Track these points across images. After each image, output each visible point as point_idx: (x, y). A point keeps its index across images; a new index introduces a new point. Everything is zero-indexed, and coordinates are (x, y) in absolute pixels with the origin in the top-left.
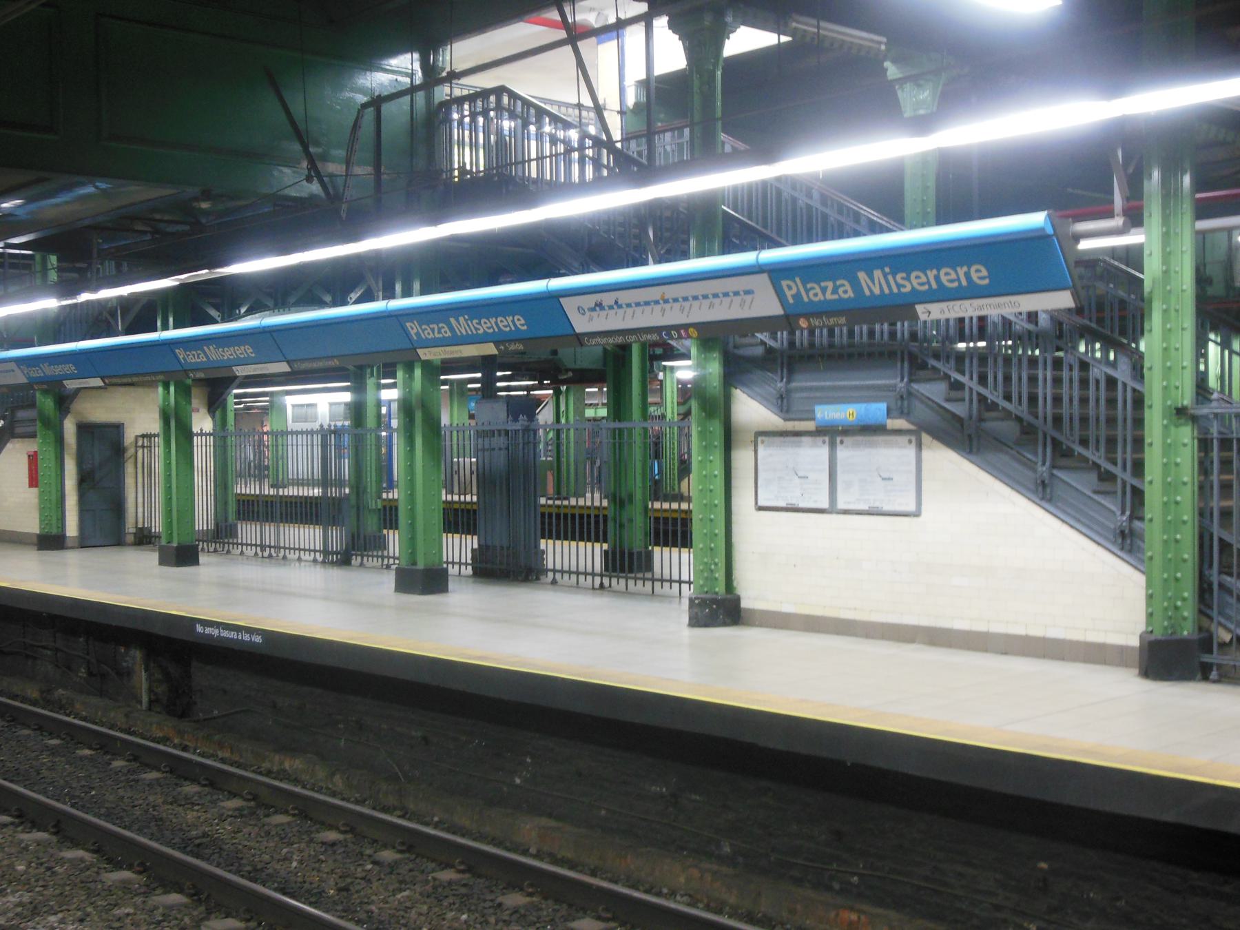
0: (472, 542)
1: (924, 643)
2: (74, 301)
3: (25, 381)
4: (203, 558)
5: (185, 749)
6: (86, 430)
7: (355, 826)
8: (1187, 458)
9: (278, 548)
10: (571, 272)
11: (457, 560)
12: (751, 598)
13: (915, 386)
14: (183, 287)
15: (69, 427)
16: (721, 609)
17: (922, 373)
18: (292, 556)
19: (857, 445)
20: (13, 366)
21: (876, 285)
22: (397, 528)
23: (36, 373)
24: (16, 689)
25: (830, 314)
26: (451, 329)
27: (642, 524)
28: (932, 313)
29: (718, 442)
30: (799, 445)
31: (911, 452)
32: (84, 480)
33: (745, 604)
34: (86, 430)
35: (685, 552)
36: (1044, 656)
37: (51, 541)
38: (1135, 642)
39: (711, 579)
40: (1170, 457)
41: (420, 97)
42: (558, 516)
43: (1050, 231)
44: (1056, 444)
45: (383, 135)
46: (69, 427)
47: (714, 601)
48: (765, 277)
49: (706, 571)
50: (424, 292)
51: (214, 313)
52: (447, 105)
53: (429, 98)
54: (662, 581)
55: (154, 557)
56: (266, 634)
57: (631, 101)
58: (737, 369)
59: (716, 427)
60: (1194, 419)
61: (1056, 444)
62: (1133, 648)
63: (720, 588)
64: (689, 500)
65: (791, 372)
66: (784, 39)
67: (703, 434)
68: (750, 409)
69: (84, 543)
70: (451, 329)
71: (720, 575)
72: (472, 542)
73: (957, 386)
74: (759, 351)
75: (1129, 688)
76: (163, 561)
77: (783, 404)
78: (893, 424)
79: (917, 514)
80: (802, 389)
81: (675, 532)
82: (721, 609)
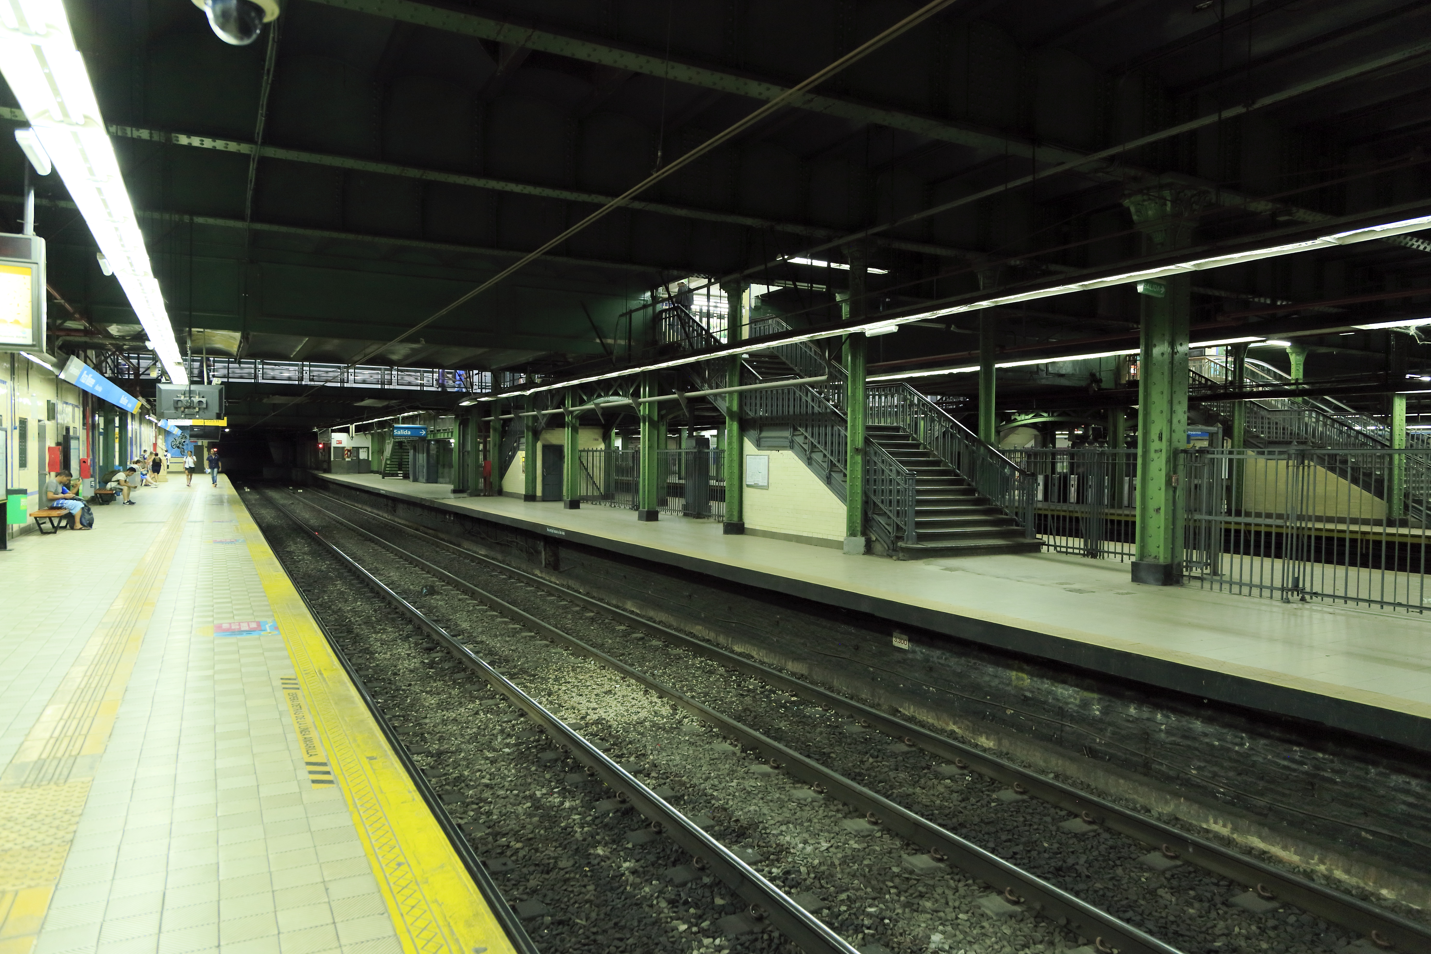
1: (355, 473)
4: (581, 505)
11: (1256, 580)
12: (748, 524)
17: (797, 433)
24: (475, 549)
33: (746, 526)
34: (545, 447)
37: (530, 497)
39: (732, 515)
42: (1071, 518)
45: (633, 324)
49: (730, 511)
53: (654, 310)
56: (566, 531)
57: (753, 305)
63: (735, 519)
65: (761, 431)
66: (773, 289)
69: (545, 499)
71: (736, 513)
72: (683, 501)
76: (640, 518)
79: (766, 488)
81: (719, 495)
82: (736, 527)
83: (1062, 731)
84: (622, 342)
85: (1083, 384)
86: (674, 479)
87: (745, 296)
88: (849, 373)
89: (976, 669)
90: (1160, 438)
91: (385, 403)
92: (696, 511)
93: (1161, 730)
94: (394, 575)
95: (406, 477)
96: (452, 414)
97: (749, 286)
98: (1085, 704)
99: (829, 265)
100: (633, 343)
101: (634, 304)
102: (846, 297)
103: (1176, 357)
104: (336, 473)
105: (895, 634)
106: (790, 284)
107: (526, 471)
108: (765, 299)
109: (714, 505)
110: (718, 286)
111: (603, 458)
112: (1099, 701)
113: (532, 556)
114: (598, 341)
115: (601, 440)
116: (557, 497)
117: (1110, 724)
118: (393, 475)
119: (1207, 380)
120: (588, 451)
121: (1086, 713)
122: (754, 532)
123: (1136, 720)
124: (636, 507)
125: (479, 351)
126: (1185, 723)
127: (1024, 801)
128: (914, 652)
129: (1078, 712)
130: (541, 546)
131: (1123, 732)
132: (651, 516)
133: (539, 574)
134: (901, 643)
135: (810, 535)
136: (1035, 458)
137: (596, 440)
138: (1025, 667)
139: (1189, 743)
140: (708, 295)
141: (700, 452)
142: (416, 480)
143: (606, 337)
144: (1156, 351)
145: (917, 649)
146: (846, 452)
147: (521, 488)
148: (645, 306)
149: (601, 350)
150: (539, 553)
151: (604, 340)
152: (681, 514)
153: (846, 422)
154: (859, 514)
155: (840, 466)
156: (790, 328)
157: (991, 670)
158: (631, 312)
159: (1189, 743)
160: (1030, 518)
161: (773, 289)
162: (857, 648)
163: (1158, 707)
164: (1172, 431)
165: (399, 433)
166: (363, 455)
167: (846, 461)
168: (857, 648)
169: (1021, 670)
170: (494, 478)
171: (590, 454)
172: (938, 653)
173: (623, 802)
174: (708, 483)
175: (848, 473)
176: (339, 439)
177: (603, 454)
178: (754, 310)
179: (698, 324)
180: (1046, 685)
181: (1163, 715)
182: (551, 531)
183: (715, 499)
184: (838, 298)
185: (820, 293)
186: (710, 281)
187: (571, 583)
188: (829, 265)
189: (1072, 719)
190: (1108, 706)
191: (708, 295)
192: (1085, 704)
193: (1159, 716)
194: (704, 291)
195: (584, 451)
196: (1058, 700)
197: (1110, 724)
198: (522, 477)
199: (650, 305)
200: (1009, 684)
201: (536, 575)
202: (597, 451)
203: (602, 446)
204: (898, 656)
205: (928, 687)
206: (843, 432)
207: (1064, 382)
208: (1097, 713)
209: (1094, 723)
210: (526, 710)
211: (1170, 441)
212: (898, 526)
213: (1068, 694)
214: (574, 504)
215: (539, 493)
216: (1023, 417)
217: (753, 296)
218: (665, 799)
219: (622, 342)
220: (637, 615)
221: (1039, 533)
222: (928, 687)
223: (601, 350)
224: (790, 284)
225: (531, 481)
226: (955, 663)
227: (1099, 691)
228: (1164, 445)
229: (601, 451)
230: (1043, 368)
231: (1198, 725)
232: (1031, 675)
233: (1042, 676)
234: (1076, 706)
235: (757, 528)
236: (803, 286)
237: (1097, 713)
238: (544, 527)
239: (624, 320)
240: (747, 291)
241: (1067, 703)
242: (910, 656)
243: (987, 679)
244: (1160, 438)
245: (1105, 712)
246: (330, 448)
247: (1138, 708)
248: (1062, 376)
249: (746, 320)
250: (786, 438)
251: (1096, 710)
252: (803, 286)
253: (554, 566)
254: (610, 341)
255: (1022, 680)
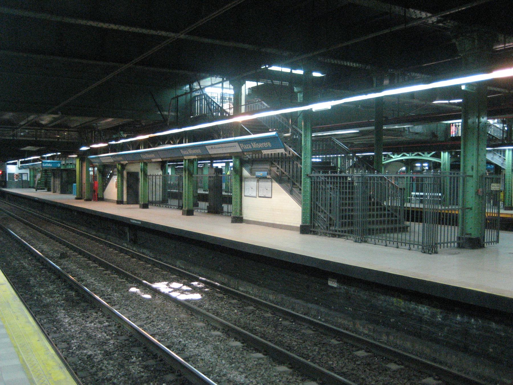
0: (207, 204)
2: (117, 143)
3: (240, 150)
4: (149, 207)
5: (160, 260)
6: (129, 173)
7: (155, 264)
8: (308, 185)
9: (228, 212)
10: (209, 140)
11: (449, 240)
12: (245, 217)
13: (272, 168)
14: (150, 138)
15: (125, 173)
16: (238, 219)
17: (273, 166)
18: (173, 207)
19: (263, 181)
20: (236, 144)
21: (255, 146)
22: (231, 204)
23: (248, 147)
25: (249, 152)
26: (252, 146)
27: (219, 200)
28: (265, 152)
29: (238, 180)
30: (267, 182)
31: (270, 183)
32: (128, 187)
33: (244, 218)
34: (129, 173)
35: (456, 227)
36: (281, 228)
37: (120, 202)
38: (299, 226)
40: (306, 184)
41: (189, 95)
43: (277, 136)
44: (293, 182)
46: (125, 173)
47: (237, 217)
48: (237, 143)
50: (144, 148)
51: (152, 146)
52: (195, 97)
54: (489, 242)
55: (229, 219)
56: (141, 221)
57: (247, 93)
58: (243, 163)
59: (238, 177)
60: (310, 177)
61: (293, 182)
62: (298, 227)
64: (231, 192)
65: (252, 164)
66: (259, 84)
67: (235, 178)
68: (246, 173)
69: (128, 203)
70: (252, 146)
72: (207, 204)
73: (278, 168)
74: (247, 159)
75: (297, 236)
76: (183, 214)
77: (251, 172)
78: (269, 177)
80: (254, 168)
81: (229, 200)
82: (238, 219)
83: (421, 330)
84: (173, 114)
85: (428, 138)
86: (200, 191)
87: (243, 87)
88: (303, 133)
89: (375, 297)
90: (472, 169)
91: (38, 148)
92: (215, 210)
93: (473, 328)
94: (45, 247)
95: (49, 190)
96: (76, 154)
97: (245, 83)
98: (434, 315)
99: (291, 71)
100: (179, 114)
101: (179, 92)
102: (300, 89)
103: (481, 124)
104: (9, 188)
105: (329, 279)
106: (269, 82)
107: (117, 186)
108: (253, 89)
109: (225, 207)
110: (228, 82)
111: (161, 180)
112: (441, 313)
113: (121, 236)
114: (159, 113)
115: (160, 169)
116: (136, 202)
117: (446, 325)
118: (41, 189)
119: (493, 136)
120: (153, 176)
121: (434, 320)
122: (249, 222)
123: (460, 323)
124: (180, 207)
125: (88, 119)
126: (486, 324)
127: (402, 369)
128: (340, 288)
129: (429, 319)
130: (127, 230)
131: (454, 330)
132: (189, 213)
133: (125, 246)
134: (332, 283)
135: (281, 223)
136: (334, 179)
137: (157, 169)
138: (402, 296)
139: (488, 334)
140: (222, 87)
141: (217, 176)
142: (55, 192)
143: (164, 111)
144: (470, 121)
145: (342, 287)
146: (301, 176)
147: (115, 198)
148: (186, 94)
149: (161, 118)
150: (125, 234)
151: (162, 113)
152: (206, 211)
153: (301, 159)
154: (308, 211)
155: (298, 184)
156: (269, 107)
157: (382, 297)
158: (177, 97)
159: (488, 334)
160: (402, 213)
161: (259, 84)
162: (308, 287)
163: (471, 315)
164: (478, 165)
165: (45, 165)
166: (25, 178)
167: (301, 182)
168: (308, 287)
169: (399, 297)
170: (99, 191)
171: (154, 177)
172: (353, 289)
173: (180, 375)
174: (221, 193)
175: (302, 188)
176: (12, 169)
177: (161, 177)
178: (248, 96)
179: (216, 104)
180: (412, 305)
181: (475, 320)
182: (133, 221)
183: (226, 203)
184: (296, 90)
185: (286, 87)
186: (223, 79)
187: (145, 251)
188: (291, 71)
189: (427, 323)
190: (445, 316)
191: (222, 87)
192: (434, 315)
193: (473, 320)
194: (220, 85)
195: (150, 175)
196: (419, 313)
197: (446, 325)
198: (115, 190)
199: (189, 93)
200: (392, 305)
201: (124, 246)
202: (158, 175)
203: (161, 173)
204: (331, 291)
205: (348, 308)
206: (299, 165)
207: (417, 137)
208: (440, 319)
209: (440, 326)
210: (122, 323)
211: (477, 171)
212: (330, 218)
213: (424, 309)
214: (145, 206)
215: (125, 199)
216: (396, 156)
217: (247, 88)
218: (203, 373)
219: (173, 114)
220: (182, 269)
221: (408, 220)
222: (348, 308)
223: (161, 118)
224: (269, 82)
225: (120, 193)
226: (363, 295)
227: (441, 308)
228: (474, 173)
229: (160, 175)
230: (407, 129)
231: (494, 325)
232: (405, 300)
233: (410, 301)
234: (429, 316)
235: (251, 219)
236: (277, 82)
237: (440, 319)
238: (129, 219)
239: (174, 101)
240: (244, 85)
241: (424, 315)
242: (338, 291)
243: (381, 302)
244: (472, 169)
245: (444, 318)
246: (6, 174)
247: (462, 316)
248: (417, 133)
249: (243, 102)
250: (267, 168)
251: (439, 318)
252: (277, 82)
253: (134, 242)
254: (166, 113)
255: (399, 303)
